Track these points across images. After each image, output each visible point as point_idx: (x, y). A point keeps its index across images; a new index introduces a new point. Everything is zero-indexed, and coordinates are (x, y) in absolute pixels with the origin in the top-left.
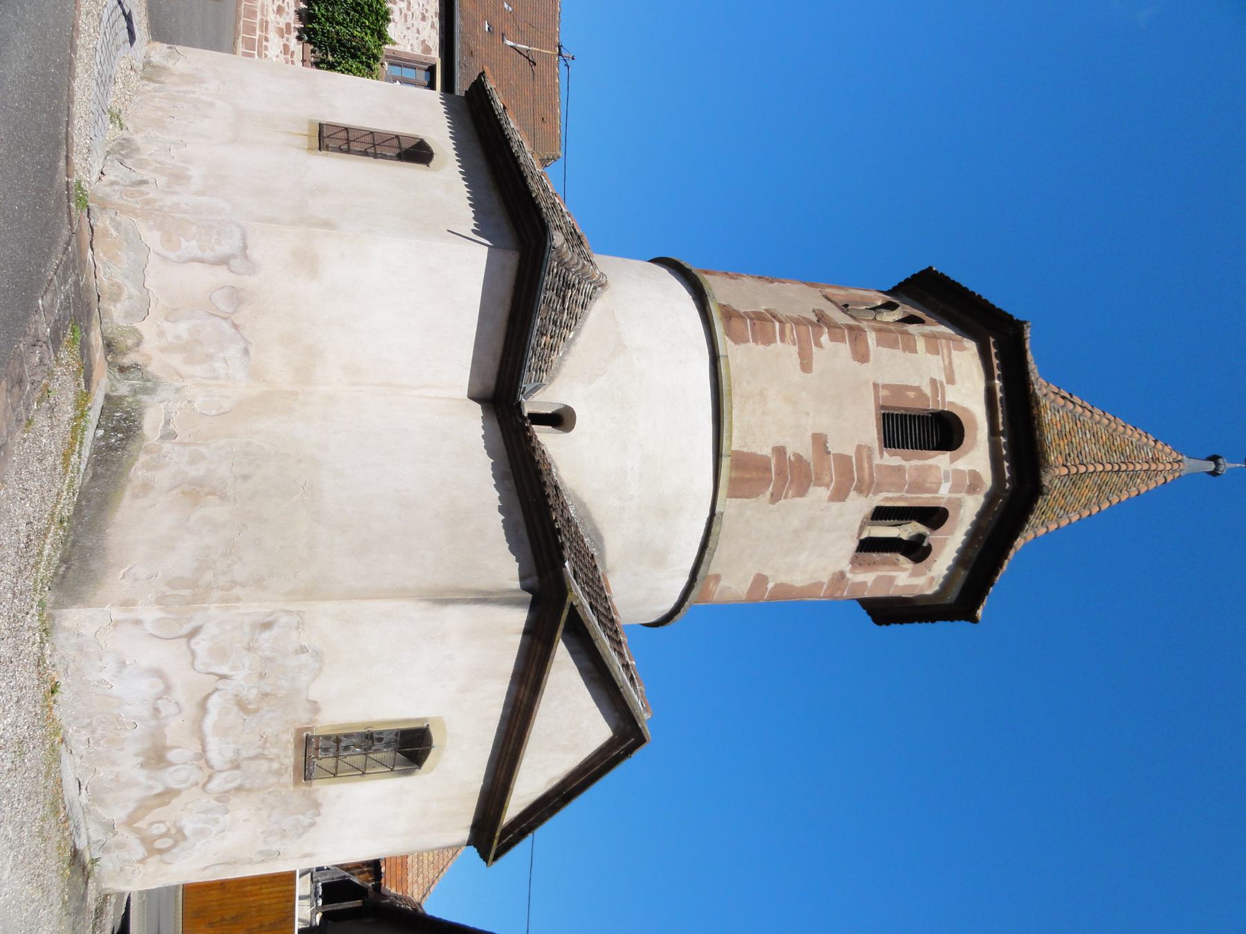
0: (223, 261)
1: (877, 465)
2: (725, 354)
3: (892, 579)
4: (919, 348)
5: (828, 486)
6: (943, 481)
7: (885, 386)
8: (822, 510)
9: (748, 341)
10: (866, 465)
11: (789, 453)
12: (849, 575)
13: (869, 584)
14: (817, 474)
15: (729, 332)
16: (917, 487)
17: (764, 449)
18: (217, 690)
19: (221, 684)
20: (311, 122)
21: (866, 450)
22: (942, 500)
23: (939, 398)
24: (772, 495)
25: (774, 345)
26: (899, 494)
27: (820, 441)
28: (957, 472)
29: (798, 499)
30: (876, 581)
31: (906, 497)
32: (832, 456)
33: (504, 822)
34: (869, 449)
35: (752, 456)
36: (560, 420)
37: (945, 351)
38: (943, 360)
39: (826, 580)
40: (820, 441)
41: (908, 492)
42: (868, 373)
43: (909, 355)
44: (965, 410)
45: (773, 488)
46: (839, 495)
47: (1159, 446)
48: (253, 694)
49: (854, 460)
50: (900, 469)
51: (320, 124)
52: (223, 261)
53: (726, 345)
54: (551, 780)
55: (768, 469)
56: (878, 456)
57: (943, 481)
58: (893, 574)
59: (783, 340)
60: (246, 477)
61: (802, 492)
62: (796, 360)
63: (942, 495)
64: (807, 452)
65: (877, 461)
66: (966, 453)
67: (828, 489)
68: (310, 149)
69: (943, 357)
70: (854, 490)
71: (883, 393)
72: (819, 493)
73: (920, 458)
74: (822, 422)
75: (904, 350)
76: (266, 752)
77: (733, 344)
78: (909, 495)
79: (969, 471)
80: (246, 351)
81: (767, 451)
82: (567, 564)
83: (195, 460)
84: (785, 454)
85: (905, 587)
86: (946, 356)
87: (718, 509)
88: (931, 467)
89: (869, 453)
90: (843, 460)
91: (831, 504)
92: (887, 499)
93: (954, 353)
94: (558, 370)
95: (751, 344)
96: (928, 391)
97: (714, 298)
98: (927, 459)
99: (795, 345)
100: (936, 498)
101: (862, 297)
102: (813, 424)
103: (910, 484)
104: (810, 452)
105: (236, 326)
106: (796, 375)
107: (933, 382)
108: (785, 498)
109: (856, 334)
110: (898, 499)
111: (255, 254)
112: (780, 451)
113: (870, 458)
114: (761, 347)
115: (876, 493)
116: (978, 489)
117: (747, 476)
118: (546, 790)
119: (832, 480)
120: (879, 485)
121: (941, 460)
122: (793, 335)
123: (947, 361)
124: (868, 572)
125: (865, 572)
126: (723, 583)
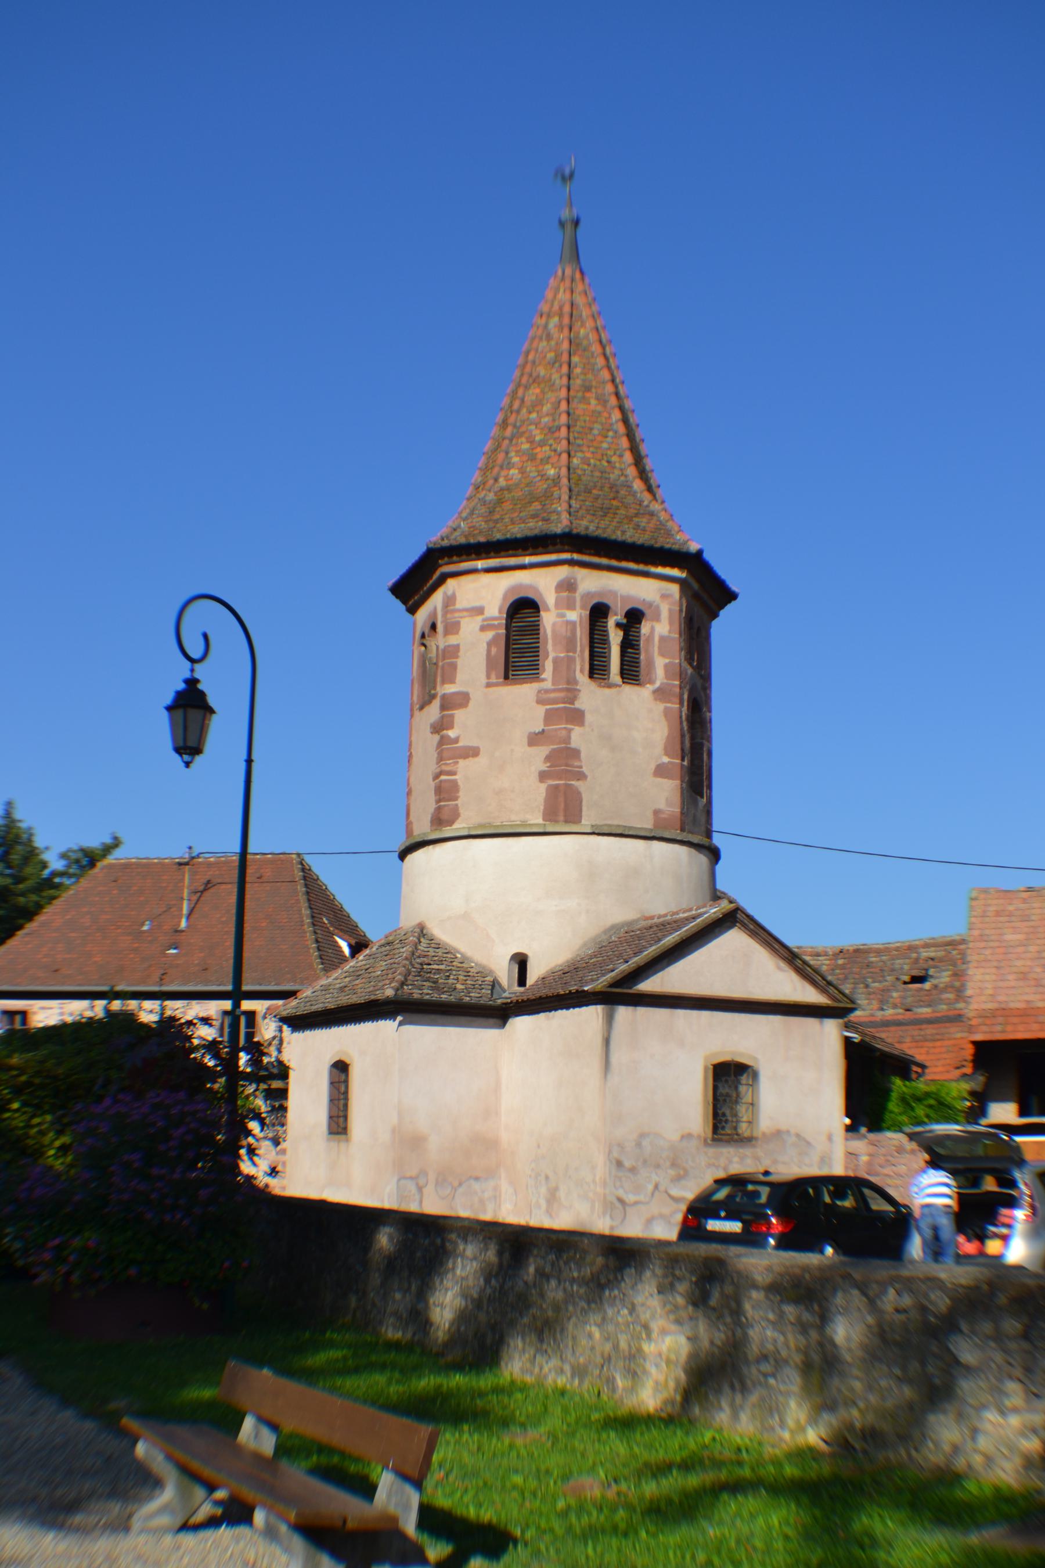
0: (420, 1189)
1: (553, 684)
2: (467, 830)
3: (662, 639)
4: (455, 643)
5: (570, 731)
6: (565, 619)
7: (488, 677)
8: (592, 730)
9: (457, 805)
10: (553, 695)
11: (544, 767)
12: (657, 684)
13: (667, 661)
14: (560, 743)
15: (451, 823)
16: (570, 644)
17: (541, 791)
18: (666, 1192)
19: (662, 1188)
20: (328, 1140)
21: (540, 695)
22: (583, 615)
23: (496, 622)
24: (578, 780)
25: (459, 781)
26: (577, 659)
27: (535, 739)
28: (557, 605)
29: (583, 755)
30: (662, 654)
31: (581, 651)
32: (546, 728)
33: (829, 1002)
34: (539, 692)
35: (547, 800)
36: (521, 962)
37: (457, 615)
38: (465, 617)
39: (661, 707)
40: (535, 739)
41: (575, 652)
42: (477, 694)
43: (461, 653)
44: (505, 597)
45: (573, 780)
46: (577, 717)
47: (545, 308)
48: (672, 1172)
49: (548, 707)
50: (556, 661)
51: (732, 596)
52: (420, 1189)
53: (459, 827)
54: (779, 968)
55: (557, 787)
56: (545, 683)
57: (565, 619)
58: (656, 639)
59: (454, 773)
60: (547, 1178)
61: (576, 753)
62: (470, 761)
63: (577, 616)
64: (543, 751)
65: (548, 685)
66: (541, 595)
67: (573, 729)
68: (347, 1140)
69: (461, 617)
70: (573, 704)
71: (494, 680)
72: (578, 737)
73: (546, 643)
74: (519, 736)
75: (457, 657)
76: (723, 1165)
77: (459, 820)
78: (578, 649)
79: (557, 592)
80: (477, 1179)
81: (543, 788)
82: (586, 989)
83: (539, 1207)
84: (544, 771)
85: (671, 623)
86: (461, 614)
87: (589, 831)
88: (553, 631)
89: (542, 692)
90: (549, 718)
91: (587, 723)
92: (582, 671)
93: (458, 606)
94: (484, 967)
95: (459, 802)
96: (490, 635)
97: (424, 834)
98: (547, 636)
99: (458, 762)
100: (580, 621)
101: (418, 666)
102: (520, 747)
103: (568, 652)
104: (542, 748)
105: (460, 1184)
106: (481, 762)
107: (483, 629)
108: (581, 767)
109: (449, 704)
110: (583, 660)
111: (414, 1173)
112: (543, 776)
113: (547, 691)
114: (461, 794)
115: (576, 682)
116: (572, 581)
117: (562, 806)
118: (790, 970)
119: (565, 728)
120: (568, 683)
121: (549, 620)
122: (450, 764)
123: (465, 614)
124: (654, 666)
125: (655, 669)
126: (662, 805)
